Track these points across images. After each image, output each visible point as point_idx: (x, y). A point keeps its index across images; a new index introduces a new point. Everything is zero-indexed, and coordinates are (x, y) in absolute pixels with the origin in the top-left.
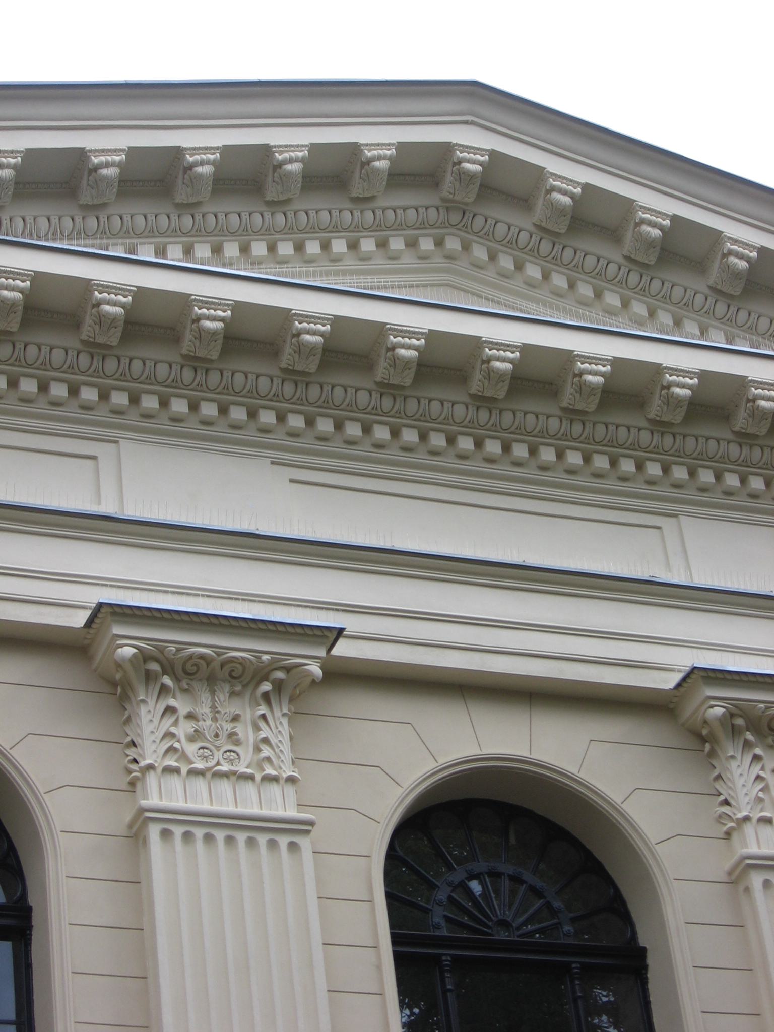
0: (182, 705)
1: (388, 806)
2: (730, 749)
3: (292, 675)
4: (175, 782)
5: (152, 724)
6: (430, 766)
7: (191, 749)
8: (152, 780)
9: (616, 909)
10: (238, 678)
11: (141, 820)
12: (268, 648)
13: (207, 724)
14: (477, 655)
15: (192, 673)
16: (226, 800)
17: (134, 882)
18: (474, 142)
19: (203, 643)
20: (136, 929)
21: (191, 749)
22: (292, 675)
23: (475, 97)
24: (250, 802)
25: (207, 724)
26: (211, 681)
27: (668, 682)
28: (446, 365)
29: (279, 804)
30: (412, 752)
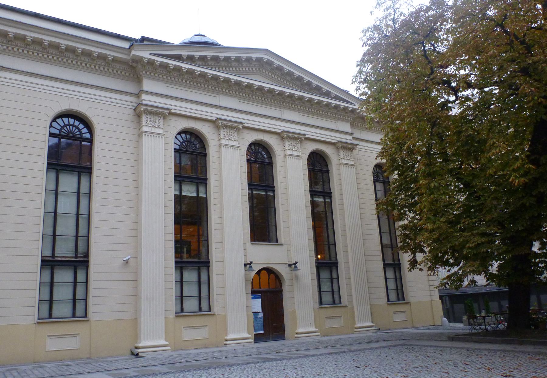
0: (226, 130)
1: (308, 153)
2: (286, 140)
3: (165, 114)
4: (147, 128)
5: (222, 132)
6: (182, 127)
7: (149, 123)
8: (144, 127)
9: (270, 157)
10: (296, 139)
11: (142, 132)
12: (236, 125)
13: (152, 120)
14: (124, 99)
15: (227, 127)
16: (153, 130)
17: (220, 152)
18: (266, 57)
19: (293, 135)
20: (220, 157)
21: (149, 123)
22: (165, 114)
23: (267, 51)
24: (156, 131)
25: (152, 120)
26: (153, 114)
27: (214, 119)
28: (260, 89)
29: (236, 144)
30: (311, 147)
